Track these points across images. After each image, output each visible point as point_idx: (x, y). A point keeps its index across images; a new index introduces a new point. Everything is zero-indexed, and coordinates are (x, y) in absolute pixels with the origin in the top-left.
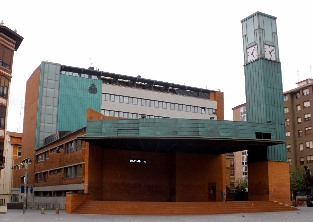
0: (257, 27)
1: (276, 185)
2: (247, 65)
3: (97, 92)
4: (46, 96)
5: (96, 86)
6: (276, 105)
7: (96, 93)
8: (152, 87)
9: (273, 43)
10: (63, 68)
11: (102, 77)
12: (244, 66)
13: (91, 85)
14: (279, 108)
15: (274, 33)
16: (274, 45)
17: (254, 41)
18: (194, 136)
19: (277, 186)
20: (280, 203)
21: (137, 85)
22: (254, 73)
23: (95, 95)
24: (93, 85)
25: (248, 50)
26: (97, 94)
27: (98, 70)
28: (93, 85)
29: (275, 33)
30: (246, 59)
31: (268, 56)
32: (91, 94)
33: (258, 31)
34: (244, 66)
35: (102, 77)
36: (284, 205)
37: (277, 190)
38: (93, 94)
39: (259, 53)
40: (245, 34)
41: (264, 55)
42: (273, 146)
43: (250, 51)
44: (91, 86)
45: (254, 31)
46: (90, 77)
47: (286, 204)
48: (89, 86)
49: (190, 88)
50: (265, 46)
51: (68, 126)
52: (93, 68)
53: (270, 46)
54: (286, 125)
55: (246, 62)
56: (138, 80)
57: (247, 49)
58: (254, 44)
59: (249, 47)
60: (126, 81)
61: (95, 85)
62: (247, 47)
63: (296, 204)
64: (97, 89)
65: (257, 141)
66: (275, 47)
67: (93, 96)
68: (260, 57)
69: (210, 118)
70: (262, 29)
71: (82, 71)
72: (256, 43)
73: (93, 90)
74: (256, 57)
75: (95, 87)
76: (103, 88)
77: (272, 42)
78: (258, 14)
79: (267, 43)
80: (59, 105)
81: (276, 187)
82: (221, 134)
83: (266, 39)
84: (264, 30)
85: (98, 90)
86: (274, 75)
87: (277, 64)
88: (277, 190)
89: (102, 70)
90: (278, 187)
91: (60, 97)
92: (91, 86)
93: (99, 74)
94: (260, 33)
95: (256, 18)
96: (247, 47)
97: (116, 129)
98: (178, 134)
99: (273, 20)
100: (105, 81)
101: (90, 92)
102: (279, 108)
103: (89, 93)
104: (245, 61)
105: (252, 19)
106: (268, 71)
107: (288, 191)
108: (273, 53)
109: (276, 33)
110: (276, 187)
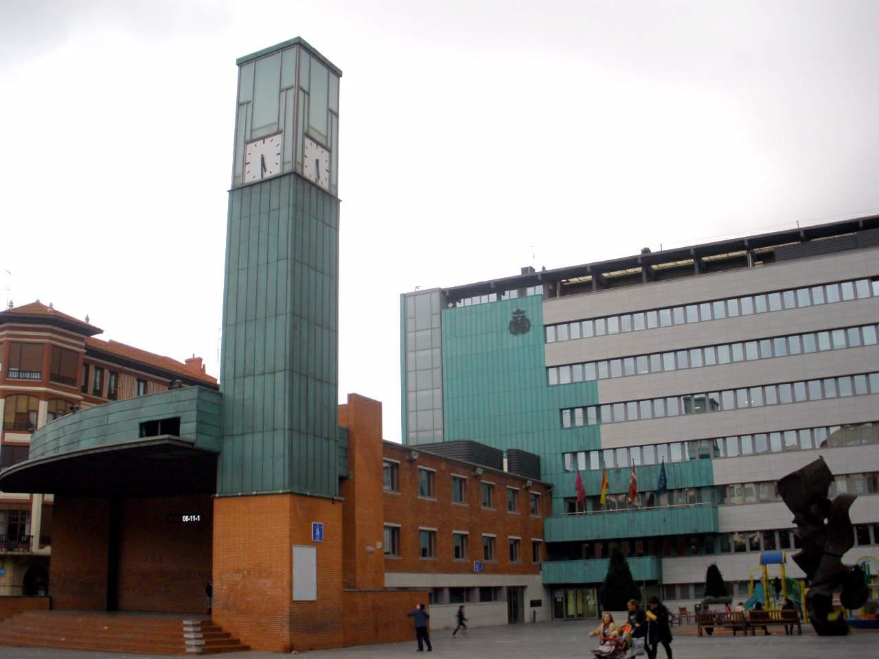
0: (289, 81)
1: (238, 571)
2: (240, 190)
3: (531, 328)
5: (525, 314)
7: (528, 330)
9: (327, 138)
10: (447, 294)
12: (229, 191)
13: (515, 313)
15: (331, 111)
16: (329, 146)
19: (241, 575)
23: (526, 335)
24: (518, 312)
25: (250, 147)
26: (531, 333)
27: (544, 268)
28: (518, 312)
29: (334, 113)
31: (309, 173)
32: (515, 338)
33: (291, 93)
34: (229, 191)
37: (239, 587)
38: (520, 336)
39: (289, 157)
41: (302, 165)
43: (256, 151)
44: (514, 318)
45: (277, 91)
46: (522, 294)
47: (837, 432)
48: (510, 319)
50: (308, 141)
51: (321, 464)
53: (318, 143)
54: (40, 381)
55: (239, 183)
57: (247, 143)
58: (274, 129)
59: (254, 137)
61: (523, 312)
62: (246, 137)
65: (144, 445)
66: (329, 151)
67: (520, 342)
68: (288, 168)
70: (304, 91)
72: (282, 126)
73: (520, 324)
74: (274, 169)
75: (524, 316)
78: (299, 44)
79: (312, 133)
80: (445, 383)
81: (238, 577)
83: (312, 123)
84: (308, 94)
85: (531, 323)
87: (330, 199)
88: (239, 587)
90: (244, 577)
92: (513, 315)
94: (297, 98)
95: (291, 54)
96: (248, 138)
99: (332, 76)
101: (511, 332)
103: (510, 336)
105: (277, 57)
108: (324, 166)
109: (337, 115)
110: (238, 577)
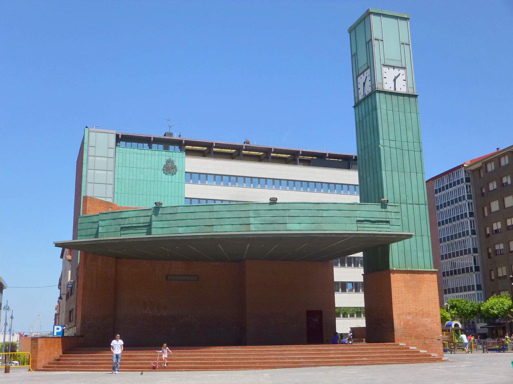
1: (409, 314)
4: (108, 185)
6: (407, 169)
8: (270, 158)
10: (120, 137)
11: (187, 147)
14: (413, 175)
15: (403, 44)
17: (366, 62)
18: (241, 231)
20: (411, 348)
21: (273, 158)
22: (368, 117)
30: (356, 96)
35: (187, 147)
36: (408, 348)
40: (354, 51)
42: (400, 243)
48: (164, 163)
49: (331, 156)
52: (171, 134)
53: (394, 67)
56: (244, 148)
60: (229, 150)
63: (451, 346)
64: (177, 166)
69: (270, 200)
71: (152, 139)
72: (369, 65)
73: (170, 168)
76: (187, 164)
77: (400, 59)
81: (409, 318)
82: (290, 226)
85: (178, 168)
86: (402, 117)
89: (185, 137)
91: (116, 183)
93: (180, 144)
97: (119, 227)
98: (215, 230)
100: (189, 153)
102: (413, 175)
104: (355, 98)
106: (390, 112)
107: (435, 324)
110: (409, 318)
